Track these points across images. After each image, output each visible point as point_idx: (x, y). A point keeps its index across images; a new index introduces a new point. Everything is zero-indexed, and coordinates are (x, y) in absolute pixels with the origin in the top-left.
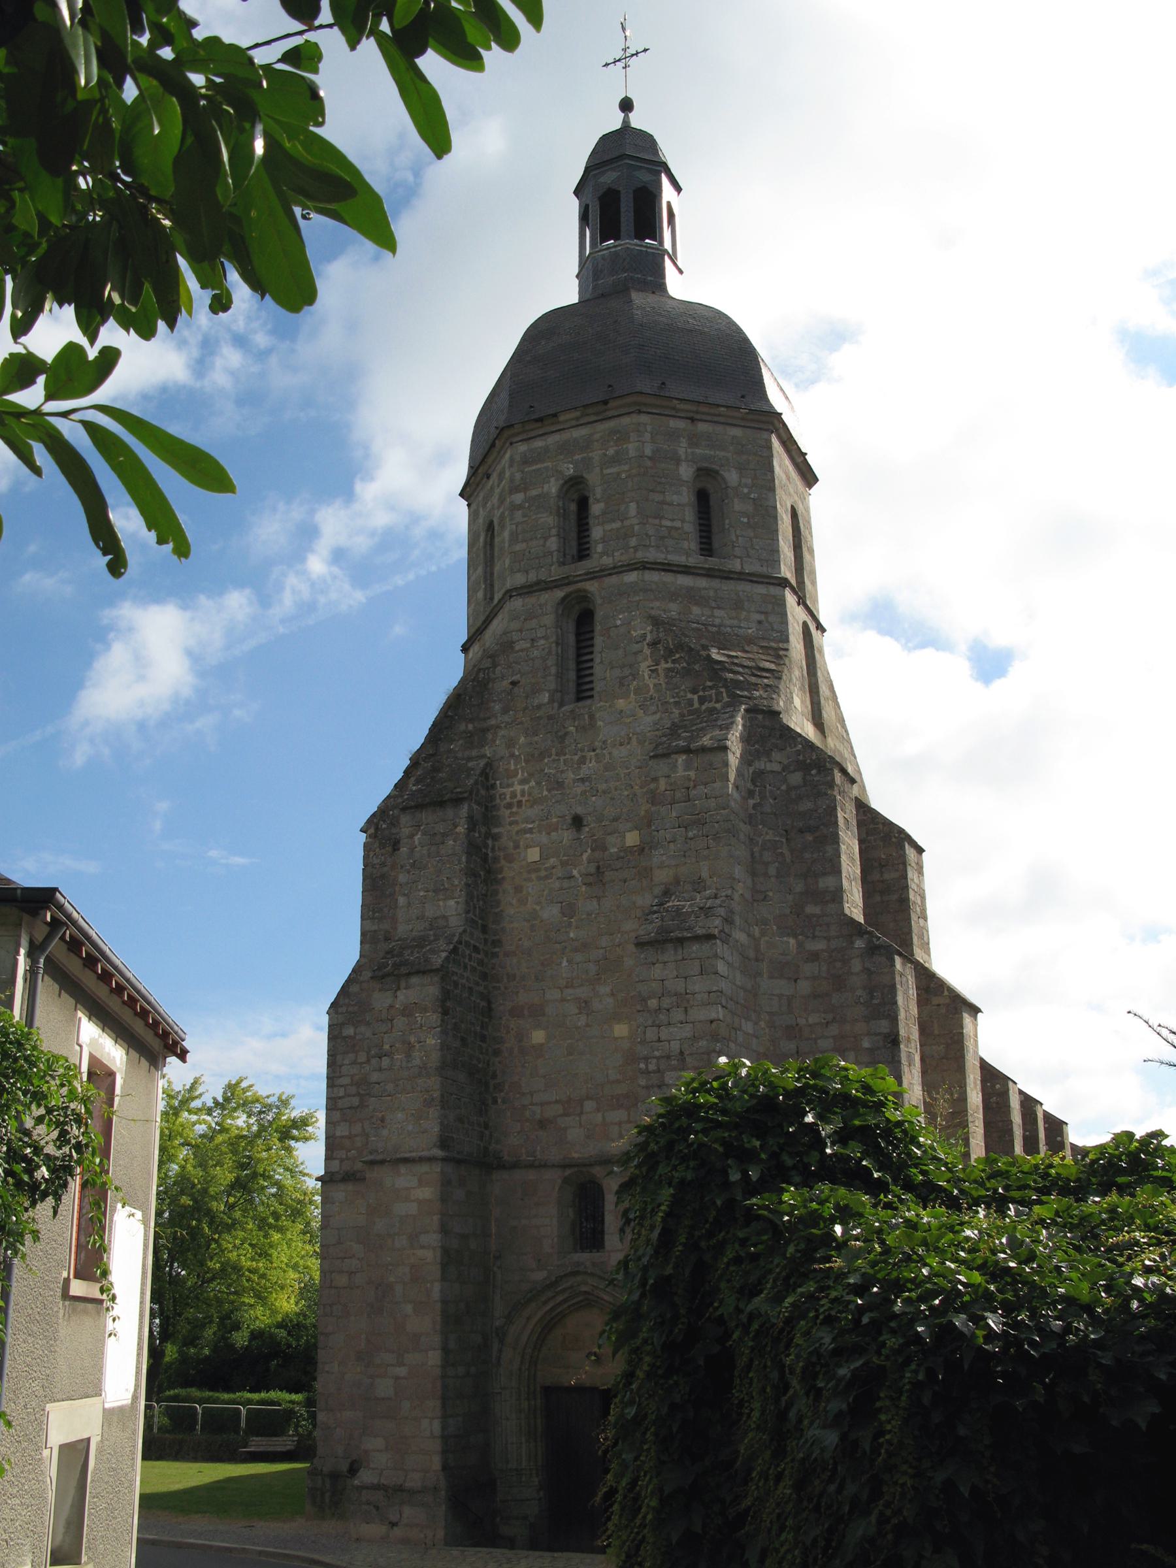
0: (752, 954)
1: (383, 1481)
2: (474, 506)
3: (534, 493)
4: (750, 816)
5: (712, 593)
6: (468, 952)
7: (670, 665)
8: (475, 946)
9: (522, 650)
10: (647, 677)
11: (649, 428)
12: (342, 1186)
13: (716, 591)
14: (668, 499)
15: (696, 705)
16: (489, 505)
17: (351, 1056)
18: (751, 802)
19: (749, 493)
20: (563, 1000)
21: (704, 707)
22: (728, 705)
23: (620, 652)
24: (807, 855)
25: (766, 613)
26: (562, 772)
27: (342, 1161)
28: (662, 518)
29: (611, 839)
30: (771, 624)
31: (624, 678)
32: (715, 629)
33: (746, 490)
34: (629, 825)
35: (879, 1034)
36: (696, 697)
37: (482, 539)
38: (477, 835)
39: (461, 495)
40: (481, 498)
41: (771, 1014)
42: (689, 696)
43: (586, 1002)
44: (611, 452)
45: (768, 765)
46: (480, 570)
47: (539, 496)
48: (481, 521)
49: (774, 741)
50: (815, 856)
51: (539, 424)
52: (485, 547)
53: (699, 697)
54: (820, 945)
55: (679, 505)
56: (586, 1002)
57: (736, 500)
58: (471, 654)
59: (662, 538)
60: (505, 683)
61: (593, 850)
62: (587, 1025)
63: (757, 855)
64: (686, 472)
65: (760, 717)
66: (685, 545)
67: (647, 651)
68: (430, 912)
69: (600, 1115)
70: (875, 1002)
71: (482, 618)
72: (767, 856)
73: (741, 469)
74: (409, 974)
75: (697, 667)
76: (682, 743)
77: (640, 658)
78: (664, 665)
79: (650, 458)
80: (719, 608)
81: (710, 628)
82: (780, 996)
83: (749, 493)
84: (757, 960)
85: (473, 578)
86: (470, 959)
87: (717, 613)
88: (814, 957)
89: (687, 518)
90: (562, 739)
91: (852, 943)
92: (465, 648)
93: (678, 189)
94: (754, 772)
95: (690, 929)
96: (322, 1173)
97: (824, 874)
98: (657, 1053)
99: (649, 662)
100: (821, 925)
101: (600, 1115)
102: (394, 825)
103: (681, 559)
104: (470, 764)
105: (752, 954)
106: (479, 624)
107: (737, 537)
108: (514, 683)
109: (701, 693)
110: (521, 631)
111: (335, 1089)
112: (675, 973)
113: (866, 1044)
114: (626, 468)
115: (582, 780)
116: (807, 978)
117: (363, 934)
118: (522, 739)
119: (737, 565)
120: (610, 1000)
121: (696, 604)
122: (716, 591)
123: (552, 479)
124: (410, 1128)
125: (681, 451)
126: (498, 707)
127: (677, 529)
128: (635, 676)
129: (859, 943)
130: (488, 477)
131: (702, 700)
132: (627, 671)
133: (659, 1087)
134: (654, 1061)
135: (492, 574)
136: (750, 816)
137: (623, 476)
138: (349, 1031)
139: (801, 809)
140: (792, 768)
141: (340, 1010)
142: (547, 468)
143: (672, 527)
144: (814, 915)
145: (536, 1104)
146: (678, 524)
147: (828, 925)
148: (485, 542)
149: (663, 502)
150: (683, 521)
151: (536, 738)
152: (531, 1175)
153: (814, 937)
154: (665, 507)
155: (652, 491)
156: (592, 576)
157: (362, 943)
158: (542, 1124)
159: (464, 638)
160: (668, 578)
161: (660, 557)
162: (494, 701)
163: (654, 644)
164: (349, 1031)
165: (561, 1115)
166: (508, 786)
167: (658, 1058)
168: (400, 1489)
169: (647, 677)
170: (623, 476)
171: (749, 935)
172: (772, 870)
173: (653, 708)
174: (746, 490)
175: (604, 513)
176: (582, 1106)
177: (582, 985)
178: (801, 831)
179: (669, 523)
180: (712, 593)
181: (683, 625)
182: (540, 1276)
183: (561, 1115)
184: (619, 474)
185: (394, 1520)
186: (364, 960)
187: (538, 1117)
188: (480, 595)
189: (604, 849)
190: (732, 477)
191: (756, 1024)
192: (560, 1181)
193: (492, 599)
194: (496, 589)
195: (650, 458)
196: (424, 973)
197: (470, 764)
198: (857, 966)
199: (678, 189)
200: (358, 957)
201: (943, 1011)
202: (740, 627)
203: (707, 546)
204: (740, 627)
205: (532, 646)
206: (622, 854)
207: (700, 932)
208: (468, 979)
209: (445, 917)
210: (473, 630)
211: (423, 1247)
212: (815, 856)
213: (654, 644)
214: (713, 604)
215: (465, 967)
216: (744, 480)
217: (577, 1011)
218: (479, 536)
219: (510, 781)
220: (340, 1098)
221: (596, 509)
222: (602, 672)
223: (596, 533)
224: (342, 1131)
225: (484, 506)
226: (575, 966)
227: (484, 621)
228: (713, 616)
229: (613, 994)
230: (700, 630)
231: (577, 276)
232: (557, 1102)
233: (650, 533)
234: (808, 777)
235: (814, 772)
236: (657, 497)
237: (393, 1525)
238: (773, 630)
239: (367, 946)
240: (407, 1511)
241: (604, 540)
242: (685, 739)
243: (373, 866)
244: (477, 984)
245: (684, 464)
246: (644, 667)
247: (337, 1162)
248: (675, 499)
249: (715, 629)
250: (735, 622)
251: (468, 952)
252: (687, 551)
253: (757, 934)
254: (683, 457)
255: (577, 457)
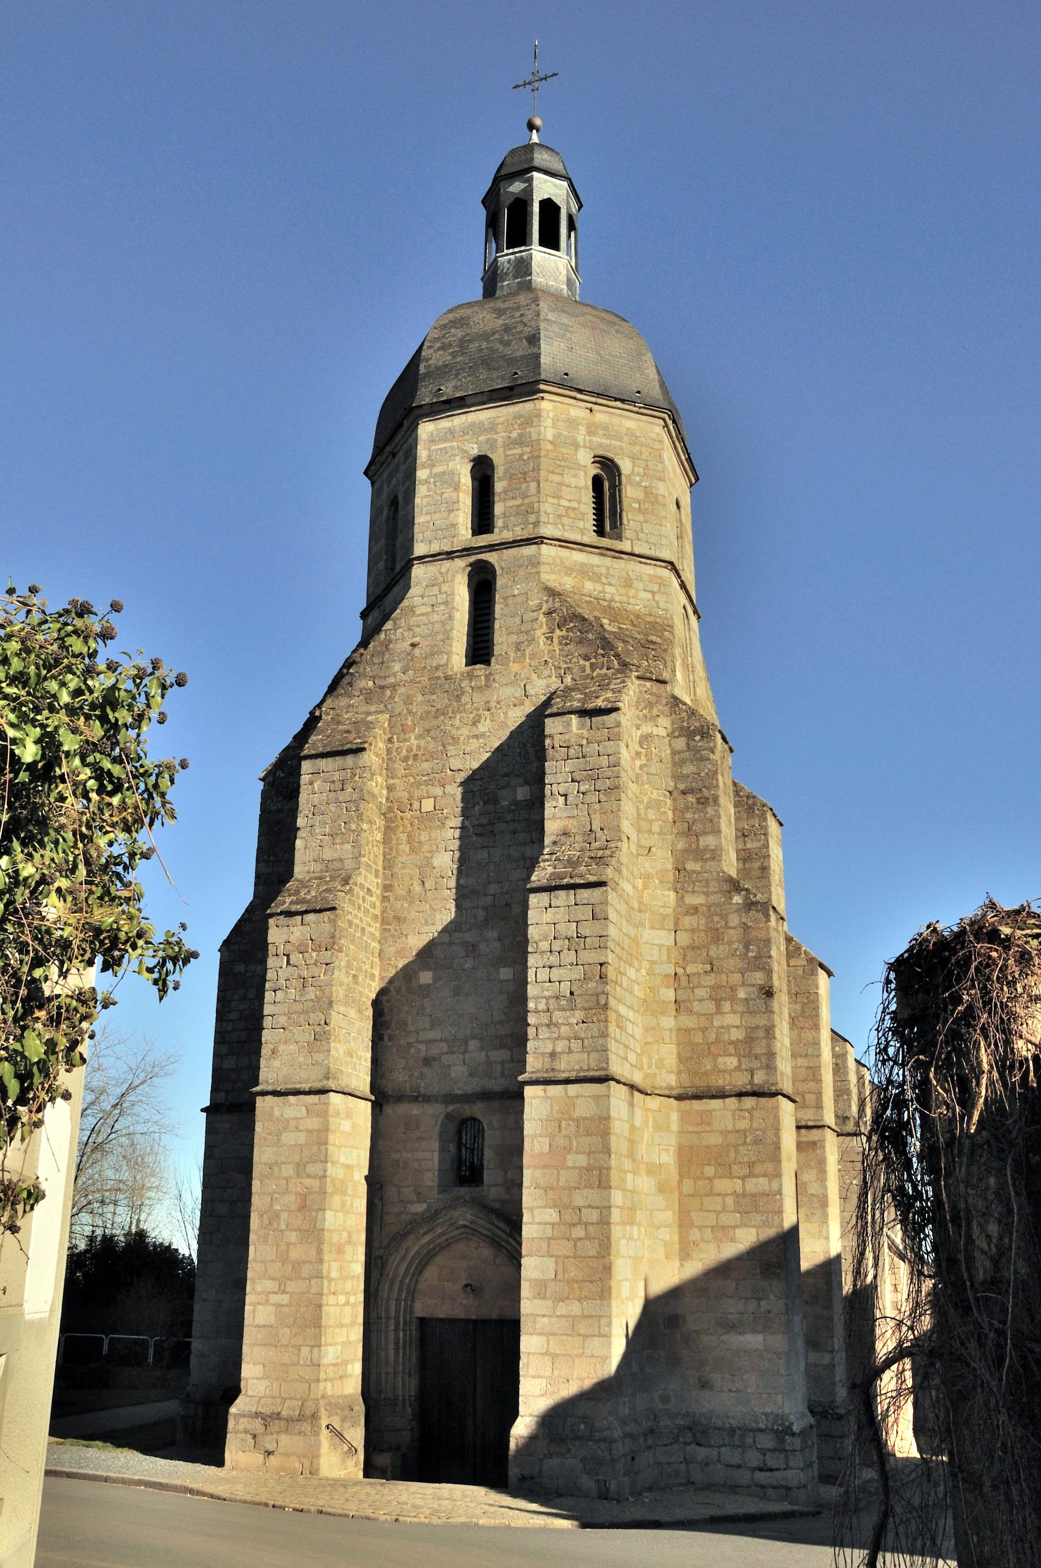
0: (636, 905)
1: (260, 1409)
2: (377, 484)
3: (438, 469)
4: (637, 776)
5: (604, 571)
6: (362, 894)
7: (564, 633)
8: (368, 889)
9: (423, 615)
10: (542, 643)
11: (551, 415)
12: (226, 1117)
13: (608, 568)
14: (566, 481)
15: (588, 671)
16: (394, 482)
17: (241, 992)
18: (638, 763)
19: (641, 481)
20: (451, 943)
21: (595, 674)
22: (618, 671)
23: (518, 620)
24: (689, 816)
25: (653, 593)
26: (458, 728)
27: (227, 1092)
28: (559, 498)
29: (503, 793)
30: (657, 602)
31: (520, 643)
32: (605, 604)
33: (638, 479)
34: (521, 780)
35: (753, 985)
36: (587, 664)
37: (385, 512)
38: (374, 784)
39: (366, 473)
40: (386, 473)
41: (653, 962)
42: (582, 662)
43: (473, 946)
44: (514, 435)
45: (655, 728)
46: (382, 542)
47: (444, 473)
48: (384, 496)
49: (660, 707)
50: (696, 816)
51: (447, 406)
52: (387, 520)
53: (592, 665)
54: (697, 900)
55: (576, 487)
56: (473, 946)
57: (628, 487)
58: (370, 620)
59: (560, 516)
60: (406, 645)
61: (485, 803)
62: (474, 968)
63: (643, 812)
64: (585, 458)
65: (648, 684)
66: (581, 524)
67: (542, 619)
68: (328, 854)
69: (483, 1053)
70: (750, 954)
71: (382, 587)
72: (651, 814)
73: (634, 458)
74: (306, 912)
75: (590, 636)
76: (576, 704)
77: (536, 626)
78: (558, 632)
79: (551, 442)
80: (610, 585)
81: (601, 602)
82: (660, 946)
83: (641, 481)
84: (640, 911)
85: (374, 550)
86: (364, 901)
87: (608, 589)
88: (694, 910)
89: (583, 500)
90: (458, 698)
91: (731, 898)
92: (364, 615)
93: (172, 781)
94: (642, 736)
95: (581, 876)
96: (208, 1104)
97: (705, 833)
98: (546, 993)
99: (545, 629)
100: (700, 881)
101: (483, 1053)
102: (292, 775)
103: (578, 538)
104: (370, 718)
105: (636, 905)
106: (378, 591)
107: (629, 521)
108: (413, 645)
109: (593, 660)
110: (422, 597)
111: (224, 1024)
112: (567, 918)
113: (742, 994)
114: (528, 450)
115: (477, 737)
116: (686, 930)
117: (258, 875)
118: (420, 698)
119: (626, 546)
120: (497, 944)
121: (589, 580)
122: (608, 568)
123: (458, 458)
124: (301, 1059)
125: (580, 439)
126: (397, 667)
127: (574, 509)
128: (532, 640)
129: (737, 899)
130: (394, 455)
131: (593, 667)
132: (523, 638)
133: (548, 1026)
134: (544, 1001)
135: (394, 546)
136: (637, 776)
137: (526, 457)
138: (241, 968)
139: (685, 772)
140: (677, 734)
141: (232, 948)
142: (452, 448)
143: (569, 508)
144: (694, 871)
145: (422, 1042)
146: (575, 505)
147: (707, 881)
148: (388, 518)
149: (561, 484)
150: (579, 502)
151: (434, 697)
152: (415, 1110)
153: (693, 892)
154: (563, 488)
155: (553, 472)
156: (491, 548)
157: (256, 884)
158: (427, 1061)
159: (363, 605)
160: (564, 553)
161: (558, 534)
162: (394, 661)
163: (549, 613)
164: (241, 968)
165: (446, 1053)
166: (405, 740)
167: (547, 998)
168: (277, 1416)
169: (542, 643)
170: (526, 457)
171: (634, 887)
172: (656, 828)
173: (546, 673)
174: (638, 479)
175: (505, 491)
176: (466, 1045)
177: (470, 930)
178: (684, 793)
179: (566, 504)
180: (604, 571)
181: (576, 597)
182: (420, 1208)
183: (446, 1053)
184: (521, 455)
185: (270, 1448)
186: (257, 901)
187: (423, 1054)
188: (381, 565)
189: (495, 801)
190: (625, 466)
191: (637, 971)
192: (442, 1117)
193: (393, 569)
194: (398, 557)
195: (551, 442)
196: (320, 911)
197: (370, 718)
198: (734, 920)
199: (172, 781)
200: (251, 898)
201: (800, 972)
202: (628, 603)
203: (600, 532)
204: (628, 603)
205: (433, 611)
206: (513, 807)
207: (592, 879)
208: (361, 920)
209: (341, 860)
210: (372, 598)
211: (309, 1176)
212: (696, 816)
213: (549, 613)
214: (604, 580)
215: (359, 908)
216: (636, 469)
217: (463, 954)
218: (382, 511)
219: (407, 736)
220: (228, 1032)
221: (499, 486)
222: (502, 639)
223: (499, 509)
224: (229, 1063)
225: (389, 482)
226: (464, 911)
227: (384, 590)
228: (603, 592)
229: (499, 939)
230: (591, 602)
231: (482, 279)
232: (442, 1040)
233: (548, 511)
234: (692, 743)
235: (698, 738)
236: (557, 478)
237: (269, 1453)
238: (659, 607)
239: (261, 888)
240: (284, 1439)
241: (505, 515)
242: (579, 700)
243: (270, 812)
244: (369, 925)
245: (582, 449)
246: (540, 633)
247: (223, 1094)
248: (573, 481)
249: (605, 604)
250: (625, 599)
251: (362, 894)
252: (585, 528)
253: (640, 887)
254: (582, 444)
255: (481, 438)
